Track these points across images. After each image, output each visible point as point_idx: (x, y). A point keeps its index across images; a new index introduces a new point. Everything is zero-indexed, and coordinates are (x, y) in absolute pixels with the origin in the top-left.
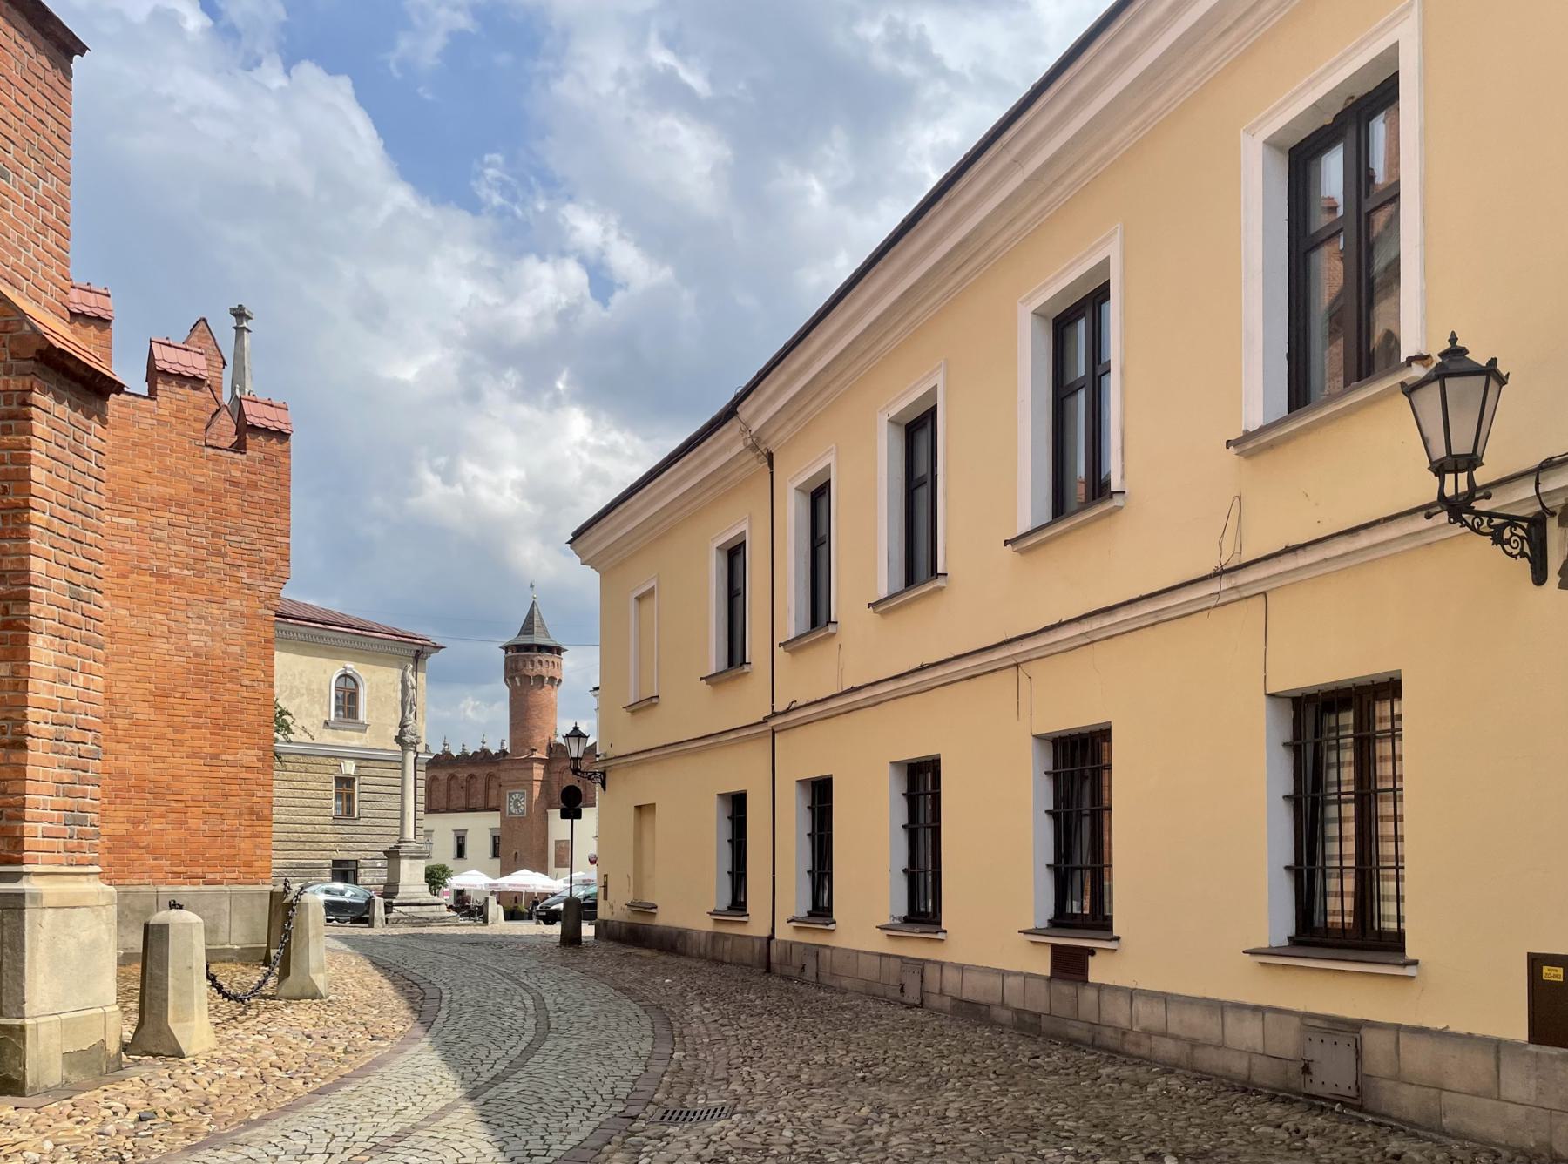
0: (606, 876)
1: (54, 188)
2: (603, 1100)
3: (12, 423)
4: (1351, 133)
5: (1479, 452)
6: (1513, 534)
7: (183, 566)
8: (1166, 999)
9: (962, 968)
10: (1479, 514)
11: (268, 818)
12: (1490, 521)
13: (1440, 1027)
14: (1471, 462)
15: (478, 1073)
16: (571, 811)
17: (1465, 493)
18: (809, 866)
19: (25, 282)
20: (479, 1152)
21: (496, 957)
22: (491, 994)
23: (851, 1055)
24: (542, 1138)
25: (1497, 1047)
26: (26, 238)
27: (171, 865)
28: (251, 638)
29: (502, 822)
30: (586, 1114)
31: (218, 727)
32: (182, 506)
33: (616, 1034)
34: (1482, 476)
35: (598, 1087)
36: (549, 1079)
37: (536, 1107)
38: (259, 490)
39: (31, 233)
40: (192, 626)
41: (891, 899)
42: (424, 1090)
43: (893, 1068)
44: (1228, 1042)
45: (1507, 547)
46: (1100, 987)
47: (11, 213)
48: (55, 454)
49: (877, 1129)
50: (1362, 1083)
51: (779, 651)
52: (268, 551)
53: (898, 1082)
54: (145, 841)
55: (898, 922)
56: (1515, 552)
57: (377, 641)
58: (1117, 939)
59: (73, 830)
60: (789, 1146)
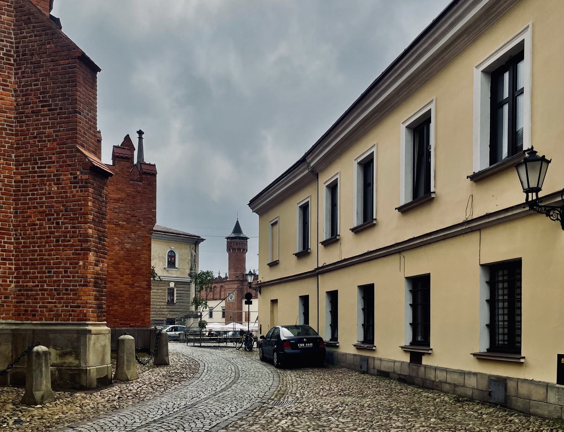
0: (261, 325)
1: (93, 115)
2: (255, 398)
3: (83, 189)
4: (511, 69)
5: (540, 186)
6: (554, 213)
7: (123, 221)
8: (446, 370)
9: (381, 360)
10: (541, 207)
11: (150, 305)
12: (545, 209)
13: (531, 379)
14: (537, 190)
15: (217, 388)
16: (249, 303)
17: (535, 200)
18: (362, 322)
19: (86, 145)
20: (217, 409)
21: (223, 353)
22: (221, 365)
23: (338, 387)
24: (235, 407)
25: (547, 386)
26: (85, 132)
27: (120, 320)
28: (144, 244)
29: (226, 304)
30: (249, 401)
31: (134, 275)
32: (123, 201)
33: (261, 379)
34: (541, 194)
35: (253, 394)
36: (238, 391)
37: (234, 399)
38: (147, 194)
39: (87, 130)
40: (126, 241)
41: (358, 336)
42: (200, 393)
43: (351, 392)
44: (466, 385)
45: (552, 217)
46: (426, 367)
47: (81, 125)
48: (95, 197)
49: (340, 408)
50: (507, 398)
51: (320, 245)
52: (149, 214)
53: (352, 396)
54: (112, 312)
55: (360, 343)
56: (554, 219)
57: (182, 238)
58: (432, 349)
59: (99, 311)
60: (311, 412)
